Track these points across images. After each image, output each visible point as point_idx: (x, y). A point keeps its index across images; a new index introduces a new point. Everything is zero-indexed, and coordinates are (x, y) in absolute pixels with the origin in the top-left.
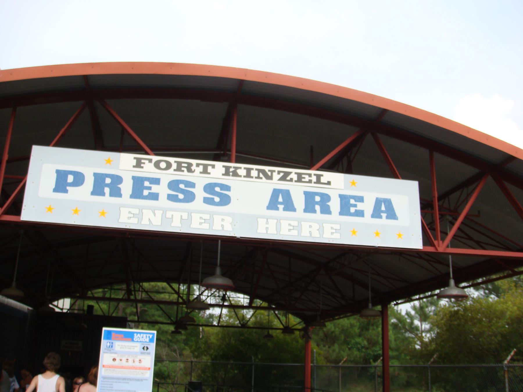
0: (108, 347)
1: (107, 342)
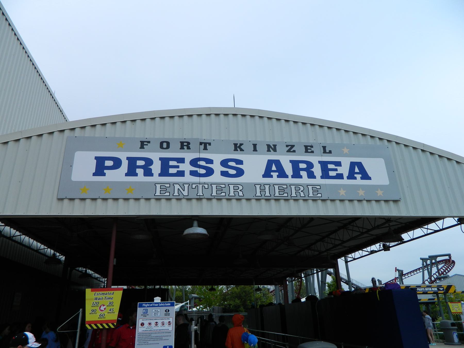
0: (144, 313)
1: (143, 310)
